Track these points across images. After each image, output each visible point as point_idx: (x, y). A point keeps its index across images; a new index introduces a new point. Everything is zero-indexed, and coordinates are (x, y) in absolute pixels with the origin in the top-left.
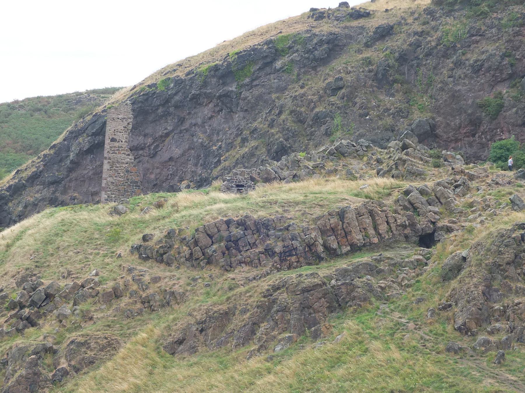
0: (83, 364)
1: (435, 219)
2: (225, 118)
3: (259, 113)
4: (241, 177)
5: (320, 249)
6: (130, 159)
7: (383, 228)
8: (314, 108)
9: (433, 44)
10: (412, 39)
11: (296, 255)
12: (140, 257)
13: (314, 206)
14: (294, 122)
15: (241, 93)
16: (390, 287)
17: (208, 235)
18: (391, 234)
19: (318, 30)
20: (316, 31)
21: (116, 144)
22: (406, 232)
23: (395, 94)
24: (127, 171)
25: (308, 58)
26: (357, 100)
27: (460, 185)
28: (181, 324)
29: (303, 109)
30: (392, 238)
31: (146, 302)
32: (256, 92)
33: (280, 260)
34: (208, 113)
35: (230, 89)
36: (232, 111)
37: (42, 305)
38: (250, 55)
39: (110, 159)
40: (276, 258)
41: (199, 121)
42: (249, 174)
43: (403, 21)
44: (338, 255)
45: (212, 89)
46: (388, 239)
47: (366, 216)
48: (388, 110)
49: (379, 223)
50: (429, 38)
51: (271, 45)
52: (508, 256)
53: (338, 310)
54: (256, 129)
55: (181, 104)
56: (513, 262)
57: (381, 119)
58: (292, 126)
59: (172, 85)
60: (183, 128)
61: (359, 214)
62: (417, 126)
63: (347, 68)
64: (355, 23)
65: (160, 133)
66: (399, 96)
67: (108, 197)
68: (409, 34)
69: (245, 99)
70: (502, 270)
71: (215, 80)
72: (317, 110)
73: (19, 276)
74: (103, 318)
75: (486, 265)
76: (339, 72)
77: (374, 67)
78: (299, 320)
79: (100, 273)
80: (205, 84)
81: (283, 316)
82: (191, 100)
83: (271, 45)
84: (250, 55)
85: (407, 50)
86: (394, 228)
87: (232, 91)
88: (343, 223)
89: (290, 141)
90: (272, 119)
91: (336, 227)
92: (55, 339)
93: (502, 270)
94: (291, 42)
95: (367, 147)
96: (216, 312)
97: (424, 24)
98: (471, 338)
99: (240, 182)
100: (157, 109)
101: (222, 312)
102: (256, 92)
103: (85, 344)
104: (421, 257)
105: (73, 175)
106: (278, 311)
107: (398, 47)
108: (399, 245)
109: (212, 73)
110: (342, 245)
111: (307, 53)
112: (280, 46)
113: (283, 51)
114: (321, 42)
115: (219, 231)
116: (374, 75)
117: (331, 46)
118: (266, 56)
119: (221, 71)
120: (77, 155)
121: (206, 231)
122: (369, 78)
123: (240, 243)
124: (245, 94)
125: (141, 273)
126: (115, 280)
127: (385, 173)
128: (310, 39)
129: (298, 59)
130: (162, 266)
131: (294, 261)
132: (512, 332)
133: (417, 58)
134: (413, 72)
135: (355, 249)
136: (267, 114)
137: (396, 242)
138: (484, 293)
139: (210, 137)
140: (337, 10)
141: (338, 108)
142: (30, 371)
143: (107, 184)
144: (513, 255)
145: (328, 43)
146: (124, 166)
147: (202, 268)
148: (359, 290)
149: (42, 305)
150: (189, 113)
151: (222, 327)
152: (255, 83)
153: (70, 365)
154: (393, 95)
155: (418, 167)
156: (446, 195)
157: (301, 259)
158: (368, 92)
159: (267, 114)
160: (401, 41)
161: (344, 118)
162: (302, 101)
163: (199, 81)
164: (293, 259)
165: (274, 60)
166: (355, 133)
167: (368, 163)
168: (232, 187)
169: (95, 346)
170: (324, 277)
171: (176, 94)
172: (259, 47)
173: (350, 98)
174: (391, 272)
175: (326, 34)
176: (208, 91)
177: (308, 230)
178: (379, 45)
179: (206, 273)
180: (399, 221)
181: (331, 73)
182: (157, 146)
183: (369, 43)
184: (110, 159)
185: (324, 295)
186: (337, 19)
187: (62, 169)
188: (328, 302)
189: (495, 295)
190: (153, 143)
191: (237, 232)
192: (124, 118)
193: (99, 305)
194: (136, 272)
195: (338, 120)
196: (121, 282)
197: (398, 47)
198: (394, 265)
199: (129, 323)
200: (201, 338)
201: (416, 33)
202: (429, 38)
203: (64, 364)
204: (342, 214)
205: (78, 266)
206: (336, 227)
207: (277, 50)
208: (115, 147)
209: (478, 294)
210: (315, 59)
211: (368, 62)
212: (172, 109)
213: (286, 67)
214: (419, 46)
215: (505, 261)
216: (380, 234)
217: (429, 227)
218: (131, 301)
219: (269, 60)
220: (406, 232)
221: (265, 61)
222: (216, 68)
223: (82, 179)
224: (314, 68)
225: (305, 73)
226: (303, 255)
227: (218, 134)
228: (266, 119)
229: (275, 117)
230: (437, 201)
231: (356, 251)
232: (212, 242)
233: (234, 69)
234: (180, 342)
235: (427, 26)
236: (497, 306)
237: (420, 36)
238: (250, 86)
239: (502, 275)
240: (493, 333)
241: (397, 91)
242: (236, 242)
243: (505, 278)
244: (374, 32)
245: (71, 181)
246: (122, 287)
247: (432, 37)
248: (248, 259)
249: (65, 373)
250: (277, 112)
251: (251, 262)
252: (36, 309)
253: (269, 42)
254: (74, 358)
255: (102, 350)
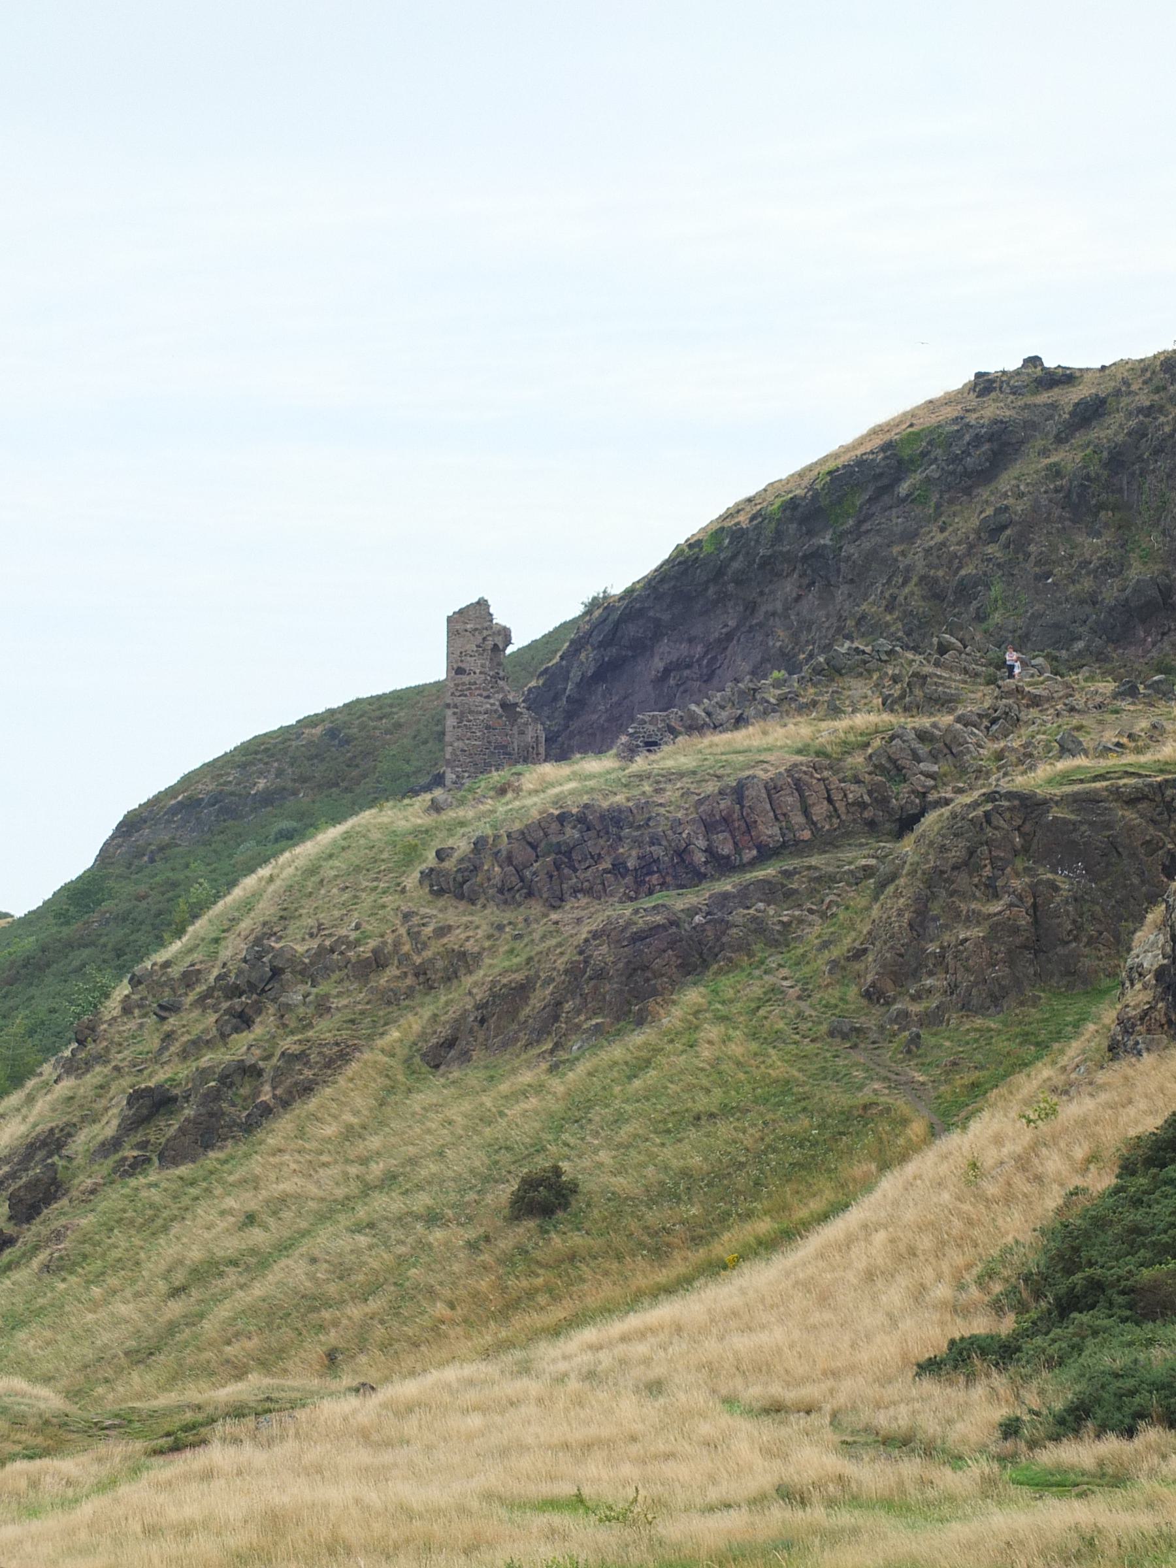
0: (295, 1093)
1: (924, 786)
2: (820, 598)
3: (872, 584)
4: (651, 728)
5: (699, 858)
6: (492, 705)
7: (820, 810)
8: (959, 568)
9: (1167, 429)
10: (1132, 423)
11: (659, 871)
12: (432, 892)
13: (707, 777)
14: (924, 598)
15: (840, 548)
16: (801, 921)
17: (529, 844)
18: (836, 821)
19: (975, 416)
20: (972, 418)
21: (465, 679)
22: (866, 815)
23: (1102, 530)
24: (488, 727)
25: (953, 473)
26: (1032, 548)
27: (999, 718)
28: (452, 1013)
29: (940, 573)
30: (839, 828)
31: (420, 972)
32: (867, 544)
33: (636, 882)
34: (791, 590)
35: (822, 542)
36: (829, 584)
37: (267, 988)
38: (852, 473)
39: (456, 706)
40: (628, 879)
41: (779, 606)
42: (663, 720)
43: (1124, 389)
44: (734, 867)
45: (790, 544)
46: (828, 831)
47: (788, 791)
48: (1085, 563)
49: (810, 802)
50: (1162, 419)
51: (889, 453)
52: (956, 853)
53: (699, 970)
54: (863, 617)
55: (744, 577)
56: (966, 864)
57: (1073, 582)
58: (919, 606)
59: (727, 541)
60: (754, 622)
61: (772, 789)
62: (1135, 591)
63: (1018, 486)
64: (1044, 398)
65: (717, 635)
66: (1108, 536)
67: (458, 777)
68: (1130, 414)
69: (848, 558)
70: (946, 881)
71: (795, 526)
72: (963, 572)
73: (251, 938)
74: (346, 1006)
75: (924, 874)
76: (1005, 495)
77: (1064, 482)
78: (620, 992)
79: (364, 925)
80: (779, 536)
81: (596, 988)
82: (762, 566)
83: (889, 453)
84: (852, 473)
85: (1124, 443)
86: (842, 809)
87: (825, 546)
88: (742, 807)
89: (915, 635)
90: (891, 595)
91: (730, 815)
92: (265, 1050)
93: (946, 881)
94: (924, 444)
95: (889, 653)
96: (504, 985)
97: (1157, 390)
98: (884, 1009)
99: (650, 736)
100: (706, 589)
101: (513, 985)
102: (867, 544)
103: (301, 1057)
104: (873, 862)
105: (574, 725)
106: (591, 978)
107: (1109, 441)
108: (851, 842)
109: (788, 513)
110: (744, 848)
111: (953, 462)
112: (906, 453)
113: (912, 461)
114: (977, 440)
115: (546, 835)
116: (1065, 497)
117: (995, 446)
118: (881, 475)
119: (800, 509)
120: (578, 685)
121: (524, 838)
122: (1056, 504)
123: (574, 856)
124: (849, 549)
125: (425, 920)
126: (382, 936)
127: (894, 702)
128: (958, 435)
129: (936, 475)
130: (462, 905)
131: (655, 882)
132: (952, 993)
133: (1140, 459)
134: (1135, 487)
135: (766, 854)
136: (884, 585)
137: (848, 834)
138: (910, 925)
139: (795, 636)
140: (1017, 373)
141: (999, 565)
142: (203, 1110)
143: (453, 753)
144: (964, 854)
145: (989, 440)
146: (481, 718)
147: (520, 905)
148: (735, 930)
149: (267, 988)
150: (762, 593)
151: (513, 1014)
152: (865, 527)
153: (274, 1096)
154: (1098, 534)
155: (949, 687)
156: (961, 740)
157: (669, 879)
158: (1054, 531)
159: (884, 585)
160: (1114, 427)
161: (1009, 584)
162: (939, 557)
163: (769, 530)
164: (655, 879)
165: (898, 480)
166: (1027, 611)
167: (877, 685)
168: (638, 746)
169: (318, 1059)
170: (682, 911)
171: (734, 557)
172: (871, 457)
173: (1019, 545)
174: (812, 892)
175: (987, 422)
176: (785, 549)
177: (680, 824)
178: (1079, 438)
179: (516, 915)
180: (851, 796)
181: (993, 498)
182: (714, 658)
183: (1063, 435)
184: (456, 706)
185: (672, 944)
186: (1015, 391)
187: (556, 714)
188: (678, 957)
189: (932, 928)
190: (706, 653)
191: (572, 833)
192: (476, 629)
193: (346, 984)
194: (415, 920)
195: (996, 590)
196: (390, 939)
197: (1109, 441)
198: (818, 879)
199: (389, 1013)
200: (481, 1036)
201: (1140, 410)
202: (1162, 419)
203: (266, 1096)
204: (739, 792)
205: (337, 913)
206: (730, 815)
207: (900, 462)
208: (463, 684)
209: (900, 927)
210: (966, 474)
211: (1055, 472)
212: (731, 587)
213: (917, 493)
214: (1145, 435)
215: (952, 861)
216: (814, 823)
217: (912, 803)
218: (397, 973)
219: (885, 481)
220: (866, 815)
221: (879, 484)
222: (792, 505)
223: (590, 731)
224: (968, 491)
225: (951, 502)
226: (670, 871)
227: (809, 630)
228: (882, 597)
229: (897, 591)
230: (946, 751)
231: (770, 858)
232: (537, 856)
233: (824, 502)
234: (450, 1043)
235: (1162, 394)
236: (933, 948)
237: (1146, 416)
238: (857, 534)
239: (947, 890)
240: (920, 998)
241: (1106, 525)
242: (568, 853)
243: (951, 896)
244: (1070, 413)
245: (571, 736)
246: (390, 948)
247: (1166, 416)
248: (586, 884)
249: (266, 1111)
250: (900, 581)
251: (591, 888)
252: (255, 996)
253: (888, 446)
254: (281, 1082)
255: (328, 1066)
